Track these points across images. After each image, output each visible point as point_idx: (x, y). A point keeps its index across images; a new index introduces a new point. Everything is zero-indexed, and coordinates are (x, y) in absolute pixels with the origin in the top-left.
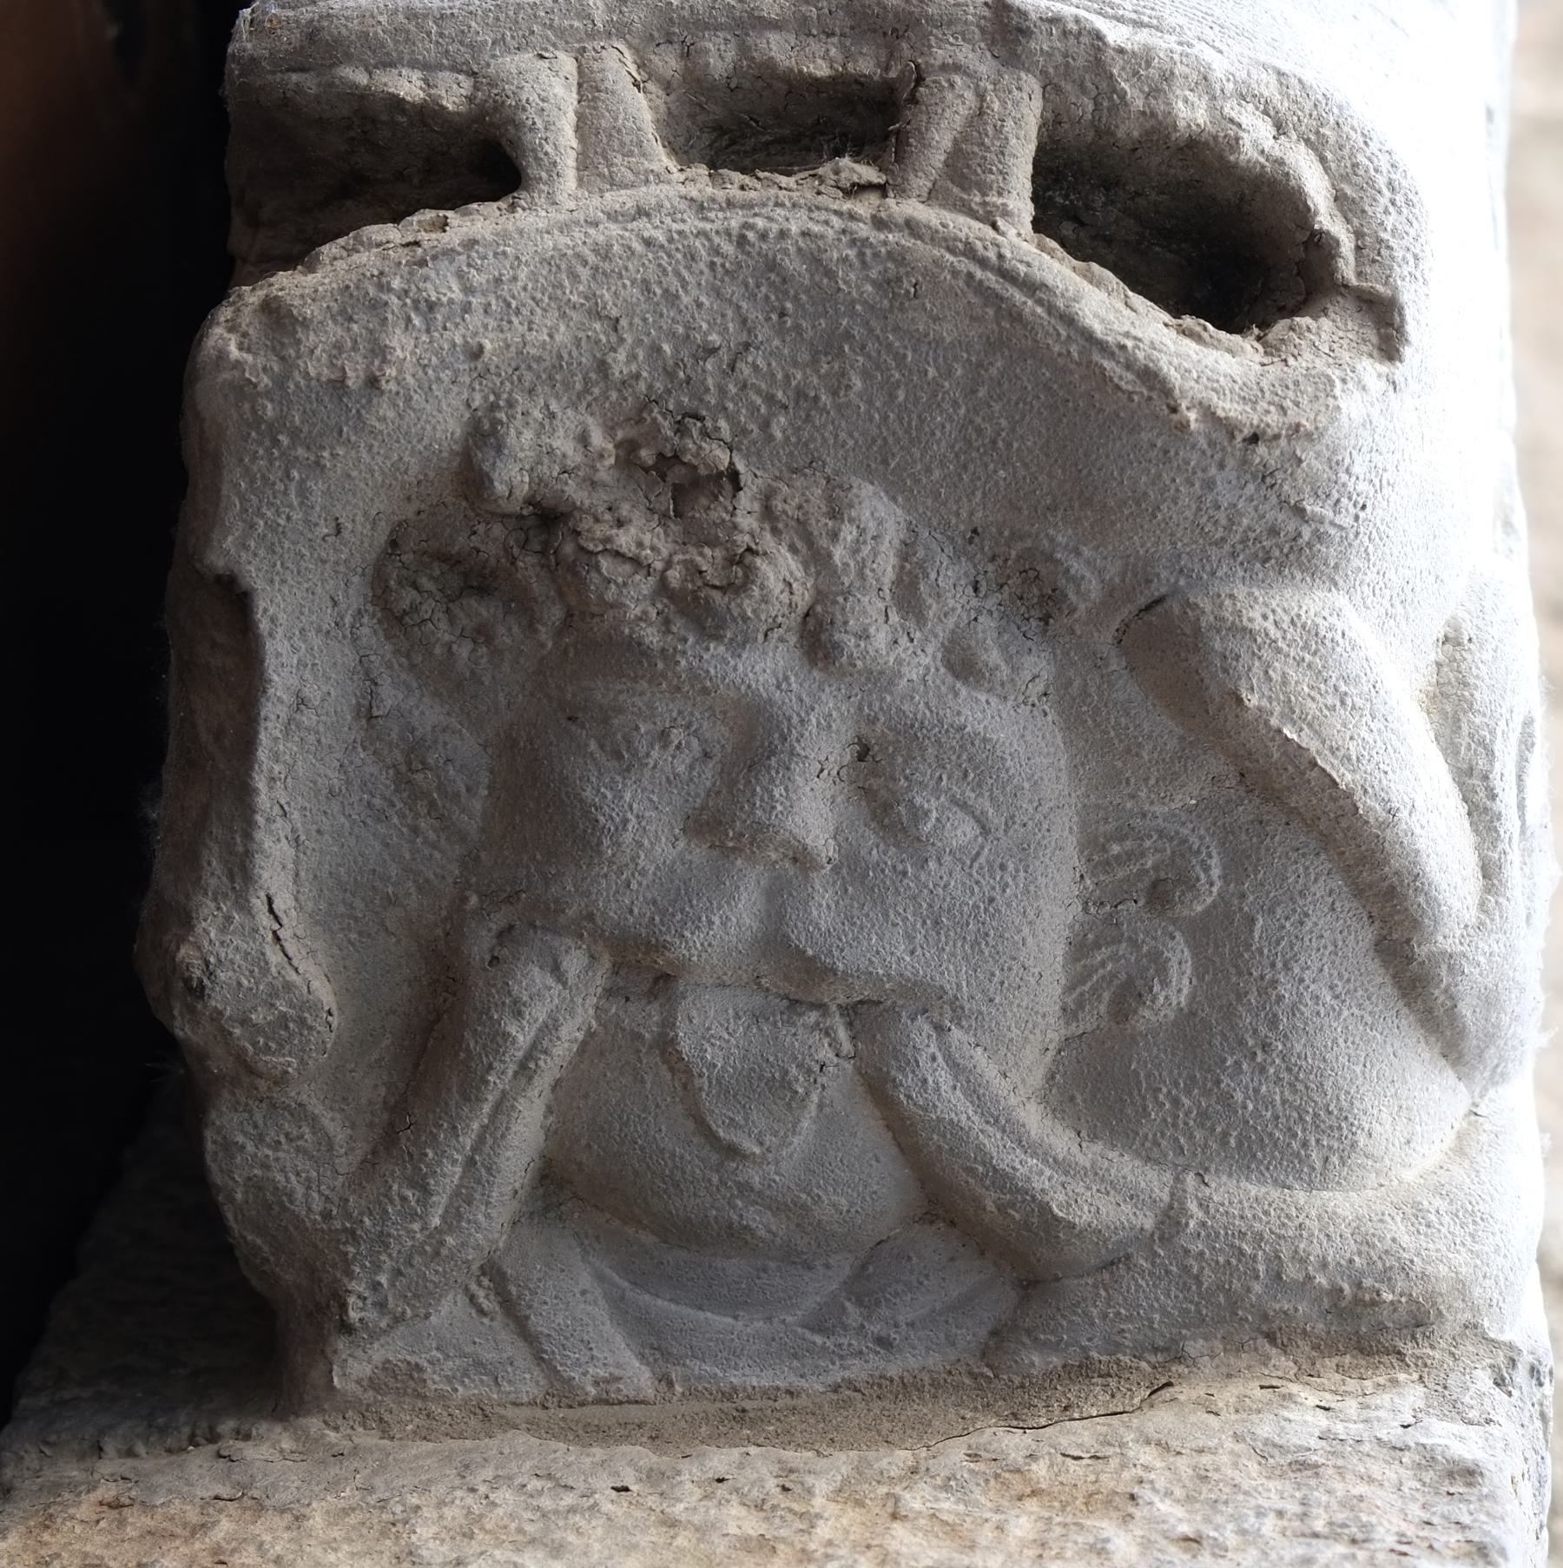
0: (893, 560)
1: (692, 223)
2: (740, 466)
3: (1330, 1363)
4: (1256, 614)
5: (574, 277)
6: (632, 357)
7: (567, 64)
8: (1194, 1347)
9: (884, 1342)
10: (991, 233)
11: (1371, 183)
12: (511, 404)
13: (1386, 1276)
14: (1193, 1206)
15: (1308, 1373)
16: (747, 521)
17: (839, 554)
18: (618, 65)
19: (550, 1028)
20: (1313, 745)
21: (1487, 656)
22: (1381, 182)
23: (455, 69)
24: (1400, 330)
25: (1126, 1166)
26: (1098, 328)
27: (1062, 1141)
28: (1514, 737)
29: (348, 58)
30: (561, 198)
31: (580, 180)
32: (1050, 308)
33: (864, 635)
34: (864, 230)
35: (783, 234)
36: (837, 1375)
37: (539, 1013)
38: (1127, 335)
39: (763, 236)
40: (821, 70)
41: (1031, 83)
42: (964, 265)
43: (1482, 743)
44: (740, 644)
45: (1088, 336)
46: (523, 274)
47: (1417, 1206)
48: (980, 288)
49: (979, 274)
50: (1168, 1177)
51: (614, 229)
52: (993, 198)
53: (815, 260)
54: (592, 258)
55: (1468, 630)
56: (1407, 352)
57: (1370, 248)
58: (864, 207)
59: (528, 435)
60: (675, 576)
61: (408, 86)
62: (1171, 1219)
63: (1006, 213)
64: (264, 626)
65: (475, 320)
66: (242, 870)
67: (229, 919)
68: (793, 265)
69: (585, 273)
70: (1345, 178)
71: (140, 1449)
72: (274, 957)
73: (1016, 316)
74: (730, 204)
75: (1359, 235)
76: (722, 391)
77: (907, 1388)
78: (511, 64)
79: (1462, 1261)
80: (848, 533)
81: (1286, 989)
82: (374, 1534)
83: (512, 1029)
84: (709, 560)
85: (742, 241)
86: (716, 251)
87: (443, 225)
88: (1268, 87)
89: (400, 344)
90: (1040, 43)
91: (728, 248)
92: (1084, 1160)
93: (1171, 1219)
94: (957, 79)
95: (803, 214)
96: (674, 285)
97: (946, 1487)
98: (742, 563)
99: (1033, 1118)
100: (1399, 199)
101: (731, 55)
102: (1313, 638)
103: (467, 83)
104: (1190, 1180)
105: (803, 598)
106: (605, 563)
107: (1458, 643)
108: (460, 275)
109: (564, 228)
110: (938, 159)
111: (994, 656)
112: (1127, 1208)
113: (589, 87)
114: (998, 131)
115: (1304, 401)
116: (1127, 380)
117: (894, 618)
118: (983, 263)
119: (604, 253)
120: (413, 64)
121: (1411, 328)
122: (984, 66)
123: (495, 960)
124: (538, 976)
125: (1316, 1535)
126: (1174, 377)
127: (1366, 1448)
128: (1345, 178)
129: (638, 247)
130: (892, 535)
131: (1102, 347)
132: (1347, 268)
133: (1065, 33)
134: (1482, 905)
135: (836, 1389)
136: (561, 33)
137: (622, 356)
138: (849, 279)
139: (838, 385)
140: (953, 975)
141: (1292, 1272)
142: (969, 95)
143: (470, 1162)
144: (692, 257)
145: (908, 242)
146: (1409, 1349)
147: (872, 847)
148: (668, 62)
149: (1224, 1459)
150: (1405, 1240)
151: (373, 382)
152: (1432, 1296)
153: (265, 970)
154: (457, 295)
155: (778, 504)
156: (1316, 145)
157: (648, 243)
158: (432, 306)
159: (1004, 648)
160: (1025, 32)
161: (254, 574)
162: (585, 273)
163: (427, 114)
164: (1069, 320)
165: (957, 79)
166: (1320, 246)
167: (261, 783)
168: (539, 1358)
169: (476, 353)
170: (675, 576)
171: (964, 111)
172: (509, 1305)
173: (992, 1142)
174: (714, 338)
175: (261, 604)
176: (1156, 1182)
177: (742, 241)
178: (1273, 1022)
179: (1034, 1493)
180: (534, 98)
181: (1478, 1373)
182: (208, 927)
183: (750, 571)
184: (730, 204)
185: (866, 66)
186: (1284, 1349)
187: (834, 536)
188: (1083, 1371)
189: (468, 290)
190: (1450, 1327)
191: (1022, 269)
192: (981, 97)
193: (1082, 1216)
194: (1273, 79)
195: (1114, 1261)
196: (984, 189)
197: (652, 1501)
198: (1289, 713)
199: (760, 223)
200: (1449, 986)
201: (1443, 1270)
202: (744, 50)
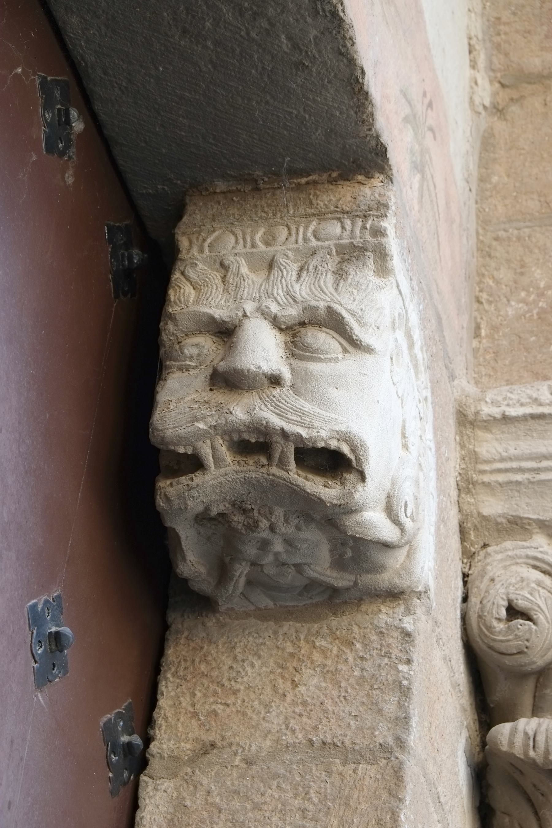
0: (283, 517)
1: (235, 476)
2: (253, 507)
3: (388, 599)
4: (347, 523)
5: (217, 488)
6: (230, 497)
7: (209, 442)
8: (364, 598)
9: (311, 598)
10: (288, 475)
11: (357, 446)
12: (211, 505)
13: (395, 588)
14: (359, 581)
15: (384, 602)
16: (256, 515)
17: (273, 520)
18: (219, 441)
19: (242, 572)
20: (362, 536)
21: (395, 499)
22: (359, 445)
23: (189, 445)
24: (365, 477)
25: (347, 576)
26: (309, 491)
27: (335, 574)
28: (403, 506)
29: (170, 445)
30: (212, 472)
31: (215, 468)
32: (300, 489)
33: (280, 530)
34: (265, 476)
35: (252, 478)
36: (304, 603)
37: (240, 571)
38: (315, 492)
39: (248, 478)
40: (253, 440)
41: (291, 444)
42: (284, 482)
43: (396, 515)
44: (259, 533)
45: (308, 493)
46: (208, 490)
47: (399, 573)
48: (287, 486)
49: (287, 484)
50: (354, 576)
51: (222, 478)
52: (288, 468)
53: (258, 481)
54: (219, 485)
55: (391, 494)
56: (367, 480)
57: (358, 460)
58: (264, 470)
59: (215, 508)
60: (246, 523)
61: (181, 450)
62: (356, 584)
63: (290, 470)
64: (178, 531)
65: (201, 498)
66: (184, 559)
67: (184, 565)
68: (254, 482)
69: (219, 488)
70: (352, 446)
71: (190, 617)
72: (193, 568)
73: (295, 490)
74: (242, 471)
75: (356, 457)
76: (247, 499)
77: (317, 605)
78: (199, 444)
79: (408, 583)
80: (274, 517)
81: (368, 554)
82: (229, 651)
83: (236, 574)
84: (251, 521)
85: (245, 479)
86: (241, 481)
87: (192, 479)
88: (335, 434)
89: (189, 503)
90: (291, 438)
91: (243, 480)
92: (339, 576)
93: (356, 584)
94: (278, 445)
95: (254, 473)
96: (235, 487)
97: (322, 638)
98: (256, 522)
99: (328, 572)
100: (362, 448)
101: (237, 436)
102: (358, 523)
103: (192, 448)
104: (358, 576)
105: (268, 526)
106: (233, 523)
107: (389, 497)
108: (197, 491)
109: (214, 479)
110: (277, 459)
111: (304, 527)
112: (348, 582)
113: (213, 448)
114: (287, 455)
115: (348, 498)
116: (316, 499)
117: (285, 525)
118: (287, 482)
119: (221, 483)
120: (182, 445)
121: (367, 476)
122: (282, 442)
123: (230, 563)
124: (238, 566)
125: (382, 656)
126: (324, 498)
127: (393, 627)
128: (352, 446)
129: (227, 482)
130: (282, 514)
131: (310, 494)
132: (354, 464)
133: (296, 436)
134: (402, 535)
135: (305, 605)
136: (206, 437)
137: (228, 497)
138: (265, 484)
139: (267, 496)
140: (308, 561)
141: (378, 589)
142: (280, 447)
143: (234, 586)
144: (236, 482)
145: (274, 478)
146: (401, 597)
147: (289, 548)
148: (227, 438)
149: (369, 630)
150: (398, 582)
151: (186, 508)
152: (404, 590)
153: (192, 570)
154: (197, 495)
155: (261, 512)
156: (346, 441)
157: (228, 481)
158: (193, 497)
159: (305, 525)
160: (289, 437)
161: (174, 526)
162: (219, 488)
163: (185, 454)
164: (304, 491)
165: (278, 445)
166: (349, 461)
167: (184, 547)
168: (253, 604)
169: (203, 502)
170: (246, 523)
171: (280, 450)
172: (247, 598)
173: (322, 578)
174: (244, 493)
175: (176, 529)
176: (352, 578)
177: (245, 479)
178: (367, 557)
179: (338, 638)
180: (204, 454)
181: (415, 599)
182: (181, 567)
183: (258, 525)
184: (242, 471)
185: (261, 440)
186: (380, 598)
187: (271, 518)
188: (345, 603)
189: (199, 493)
190: (408, 592)
191: (294, 482)
192: (283, 447)
193: (340, 585)
194: (336, 433)
195: (348, 589)
196: (286, 466)
197: (274, 641)
198: (357, 533)
199: (247, 475)
200: (494, 160)
201: (405, 585)
202: (240, 436)
